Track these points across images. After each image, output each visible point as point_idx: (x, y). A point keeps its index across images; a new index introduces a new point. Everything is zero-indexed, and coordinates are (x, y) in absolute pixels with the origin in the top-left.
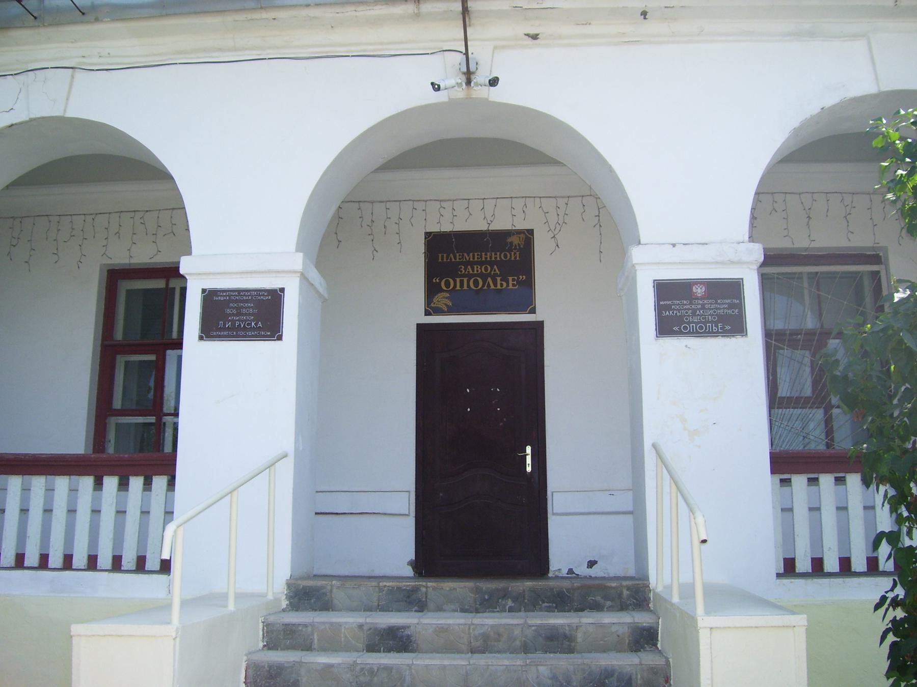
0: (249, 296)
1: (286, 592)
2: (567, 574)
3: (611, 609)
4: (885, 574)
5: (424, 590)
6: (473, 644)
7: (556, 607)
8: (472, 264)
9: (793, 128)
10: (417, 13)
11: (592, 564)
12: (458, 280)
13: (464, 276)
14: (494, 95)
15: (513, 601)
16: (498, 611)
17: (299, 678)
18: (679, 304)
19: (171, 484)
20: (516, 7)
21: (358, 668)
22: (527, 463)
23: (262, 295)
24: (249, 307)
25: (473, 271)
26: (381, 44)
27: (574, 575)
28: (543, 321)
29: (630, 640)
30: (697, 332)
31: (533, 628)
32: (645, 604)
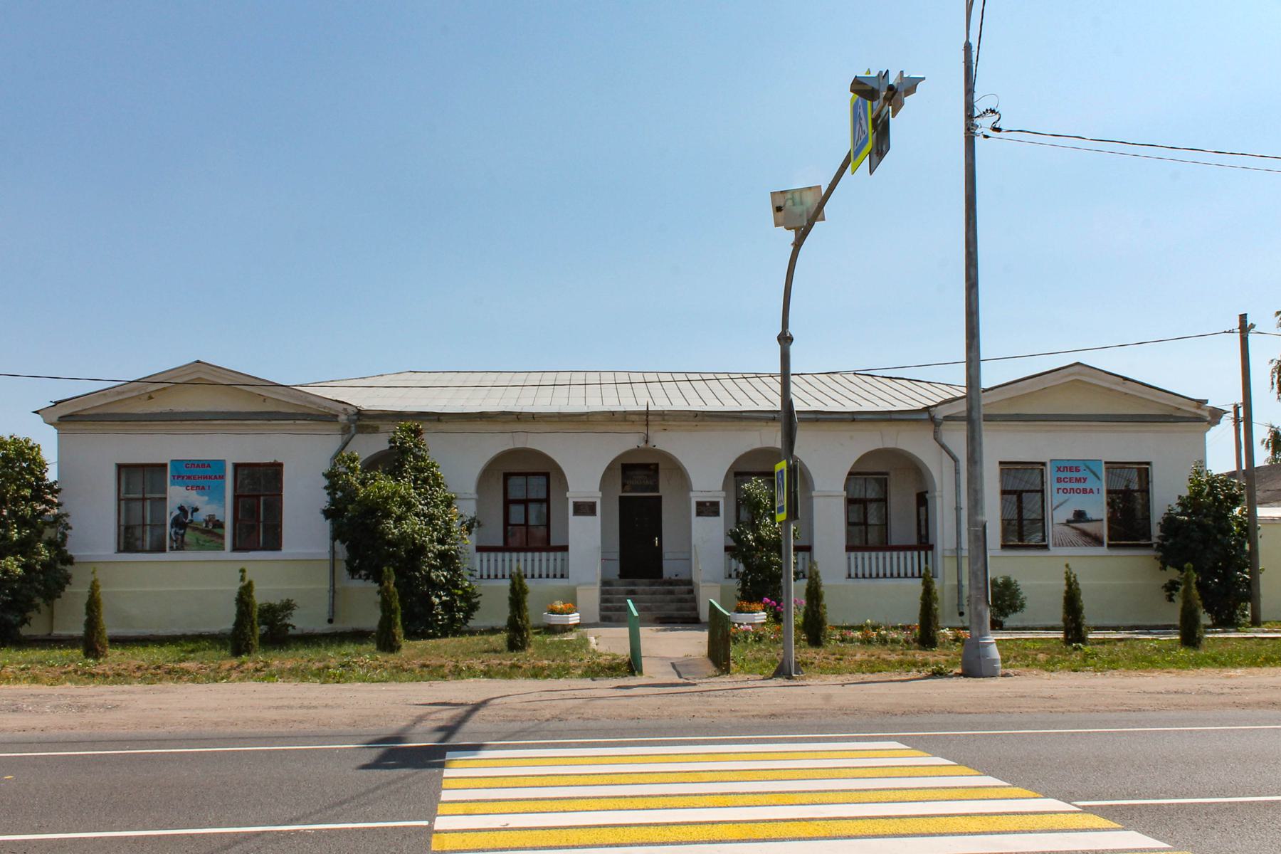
11: (676, 575)
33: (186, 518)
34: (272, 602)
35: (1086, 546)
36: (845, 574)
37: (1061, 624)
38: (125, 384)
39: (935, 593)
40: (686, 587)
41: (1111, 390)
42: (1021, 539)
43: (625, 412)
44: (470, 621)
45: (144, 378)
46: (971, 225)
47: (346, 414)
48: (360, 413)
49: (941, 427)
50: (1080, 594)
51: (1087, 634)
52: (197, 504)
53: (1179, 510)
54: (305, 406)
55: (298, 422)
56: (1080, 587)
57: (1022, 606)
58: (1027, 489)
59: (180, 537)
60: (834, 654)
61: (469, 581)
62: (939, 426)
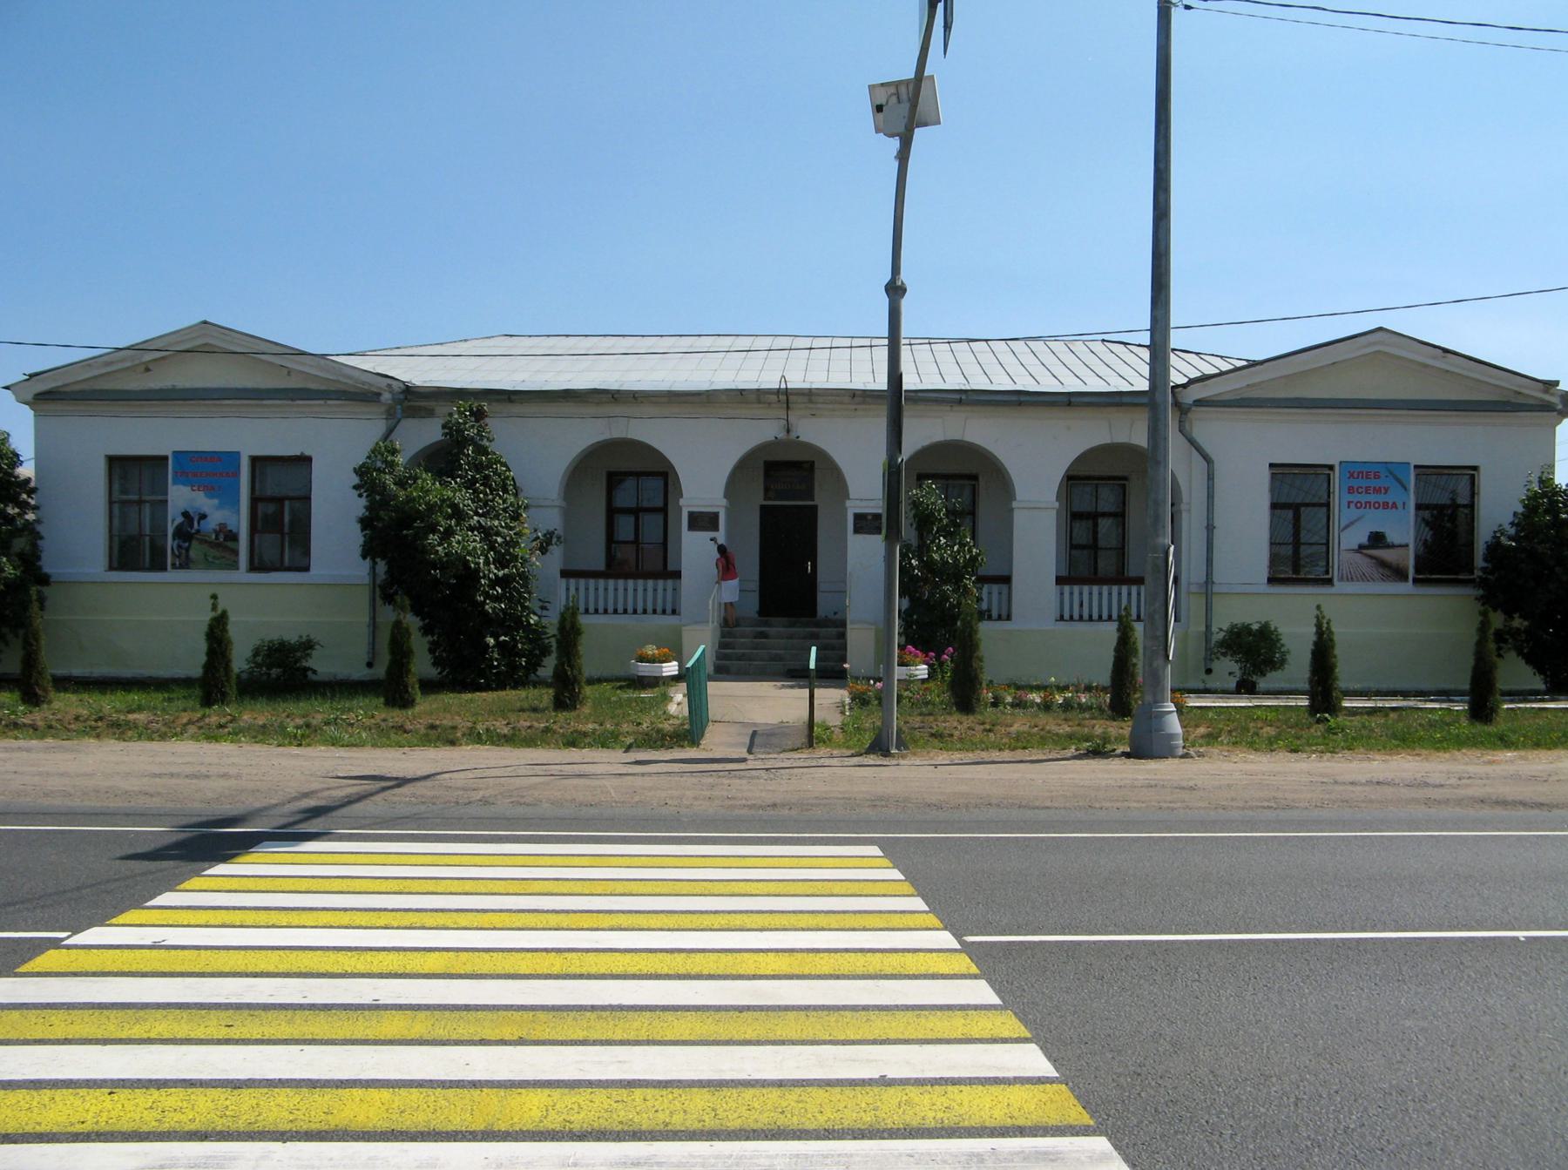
4: (1114, 621)
33: (192, 527)
34: (285, 639)
35: (1384, 581)
36: (1055, 614)
37: (1307, 687)
38: (112, 353)
39: (1134, 643)
40: (836, 629)
41: (1426, 366)
42: (1296, 569)
43: (758, 390)
44: (539, 668)
45: (137, 344)
46: (1163, 132)
47: (390, 392)
48: (409, 391)
49: (1189, 415)
50: (1333, 647)
51: (1340, 700)
52: (206, 509)
53: (1512, 531)
54: (339, 381)
55: (329, 402)
56: (1336, 638)
57: (1283, 662)
58: (1307, 501)
59: (184, 551)
60: (983, 724)
61: (540, 617)
62: (1186, 414)
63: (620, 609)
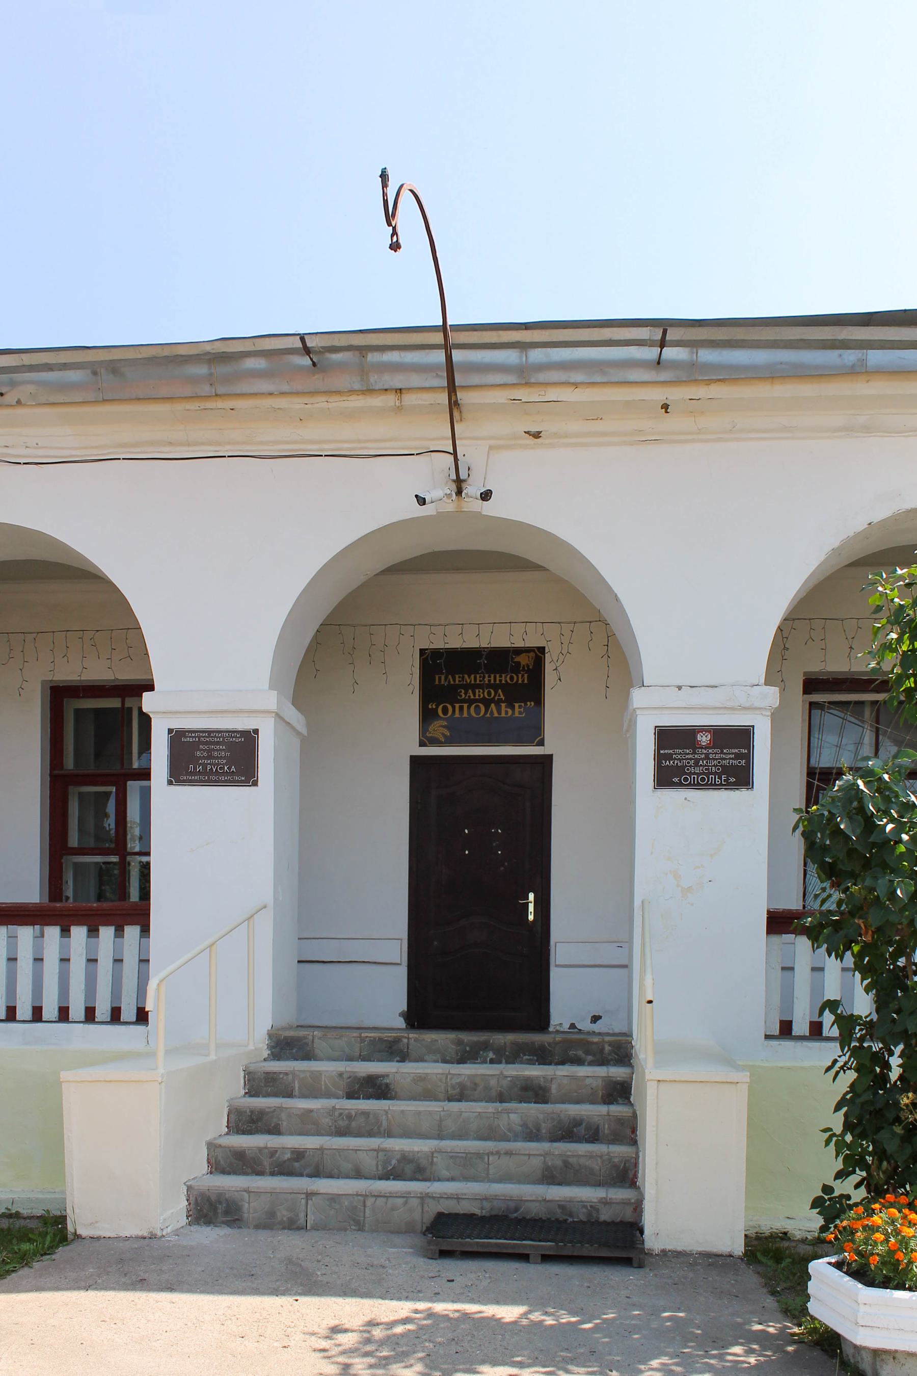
0: (220, 737)
1: (267, 1042)
2: (569, 1029)
3: (591, 1064)
5: (405, 1041)
6: (450, 1092)
7: (537, 1060)
8: (474, 687)
9: (831, 549)
10: (398, 407)
11: (595, 1019)
12: (457, 706)
13: (464, 701)
14: (488, 508)
15: (494, 1053)
16: (479, 1063)
17: (280, 1123)
18: (681, 753)
19: (145, 930)
20: (514, 400)
21: (337, 1113)
22: (529, 911)
23: (234, 737)
24: (220, 750)
25: (474, 695)
26: (359, 441)
27: (576, 1030)
28: (552, 755)
29: (603, 1093)
30: (698, 784)
31: (509, 1079)
32: (626, 1059)
63: (103, 1011)
